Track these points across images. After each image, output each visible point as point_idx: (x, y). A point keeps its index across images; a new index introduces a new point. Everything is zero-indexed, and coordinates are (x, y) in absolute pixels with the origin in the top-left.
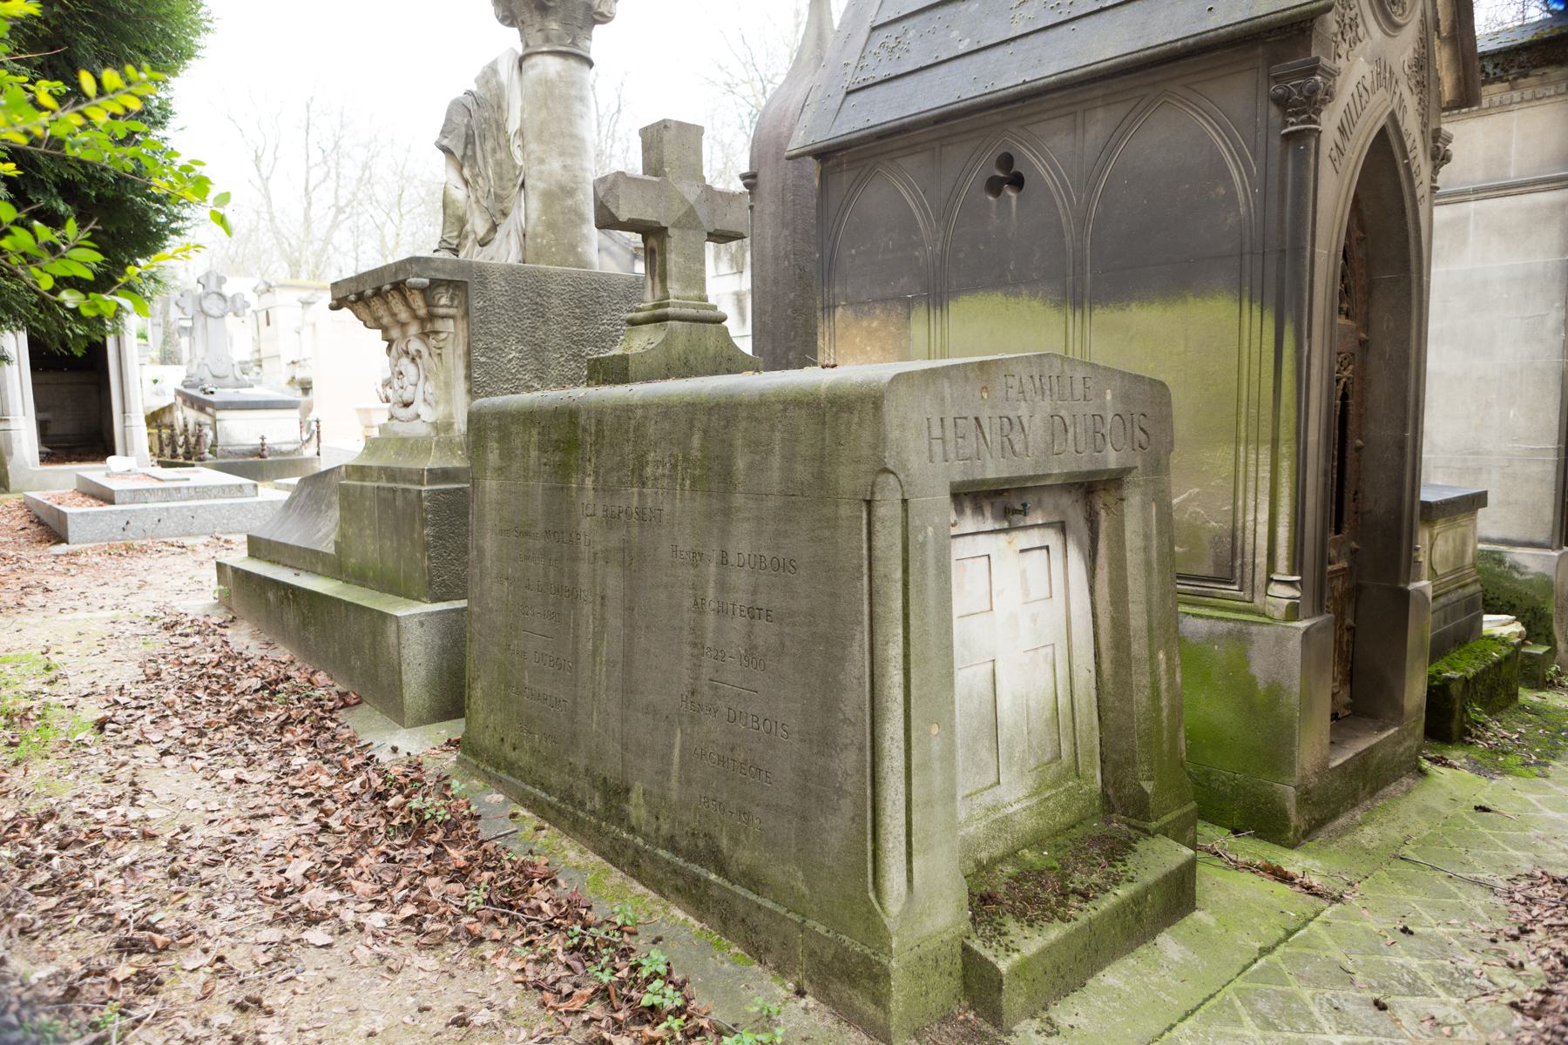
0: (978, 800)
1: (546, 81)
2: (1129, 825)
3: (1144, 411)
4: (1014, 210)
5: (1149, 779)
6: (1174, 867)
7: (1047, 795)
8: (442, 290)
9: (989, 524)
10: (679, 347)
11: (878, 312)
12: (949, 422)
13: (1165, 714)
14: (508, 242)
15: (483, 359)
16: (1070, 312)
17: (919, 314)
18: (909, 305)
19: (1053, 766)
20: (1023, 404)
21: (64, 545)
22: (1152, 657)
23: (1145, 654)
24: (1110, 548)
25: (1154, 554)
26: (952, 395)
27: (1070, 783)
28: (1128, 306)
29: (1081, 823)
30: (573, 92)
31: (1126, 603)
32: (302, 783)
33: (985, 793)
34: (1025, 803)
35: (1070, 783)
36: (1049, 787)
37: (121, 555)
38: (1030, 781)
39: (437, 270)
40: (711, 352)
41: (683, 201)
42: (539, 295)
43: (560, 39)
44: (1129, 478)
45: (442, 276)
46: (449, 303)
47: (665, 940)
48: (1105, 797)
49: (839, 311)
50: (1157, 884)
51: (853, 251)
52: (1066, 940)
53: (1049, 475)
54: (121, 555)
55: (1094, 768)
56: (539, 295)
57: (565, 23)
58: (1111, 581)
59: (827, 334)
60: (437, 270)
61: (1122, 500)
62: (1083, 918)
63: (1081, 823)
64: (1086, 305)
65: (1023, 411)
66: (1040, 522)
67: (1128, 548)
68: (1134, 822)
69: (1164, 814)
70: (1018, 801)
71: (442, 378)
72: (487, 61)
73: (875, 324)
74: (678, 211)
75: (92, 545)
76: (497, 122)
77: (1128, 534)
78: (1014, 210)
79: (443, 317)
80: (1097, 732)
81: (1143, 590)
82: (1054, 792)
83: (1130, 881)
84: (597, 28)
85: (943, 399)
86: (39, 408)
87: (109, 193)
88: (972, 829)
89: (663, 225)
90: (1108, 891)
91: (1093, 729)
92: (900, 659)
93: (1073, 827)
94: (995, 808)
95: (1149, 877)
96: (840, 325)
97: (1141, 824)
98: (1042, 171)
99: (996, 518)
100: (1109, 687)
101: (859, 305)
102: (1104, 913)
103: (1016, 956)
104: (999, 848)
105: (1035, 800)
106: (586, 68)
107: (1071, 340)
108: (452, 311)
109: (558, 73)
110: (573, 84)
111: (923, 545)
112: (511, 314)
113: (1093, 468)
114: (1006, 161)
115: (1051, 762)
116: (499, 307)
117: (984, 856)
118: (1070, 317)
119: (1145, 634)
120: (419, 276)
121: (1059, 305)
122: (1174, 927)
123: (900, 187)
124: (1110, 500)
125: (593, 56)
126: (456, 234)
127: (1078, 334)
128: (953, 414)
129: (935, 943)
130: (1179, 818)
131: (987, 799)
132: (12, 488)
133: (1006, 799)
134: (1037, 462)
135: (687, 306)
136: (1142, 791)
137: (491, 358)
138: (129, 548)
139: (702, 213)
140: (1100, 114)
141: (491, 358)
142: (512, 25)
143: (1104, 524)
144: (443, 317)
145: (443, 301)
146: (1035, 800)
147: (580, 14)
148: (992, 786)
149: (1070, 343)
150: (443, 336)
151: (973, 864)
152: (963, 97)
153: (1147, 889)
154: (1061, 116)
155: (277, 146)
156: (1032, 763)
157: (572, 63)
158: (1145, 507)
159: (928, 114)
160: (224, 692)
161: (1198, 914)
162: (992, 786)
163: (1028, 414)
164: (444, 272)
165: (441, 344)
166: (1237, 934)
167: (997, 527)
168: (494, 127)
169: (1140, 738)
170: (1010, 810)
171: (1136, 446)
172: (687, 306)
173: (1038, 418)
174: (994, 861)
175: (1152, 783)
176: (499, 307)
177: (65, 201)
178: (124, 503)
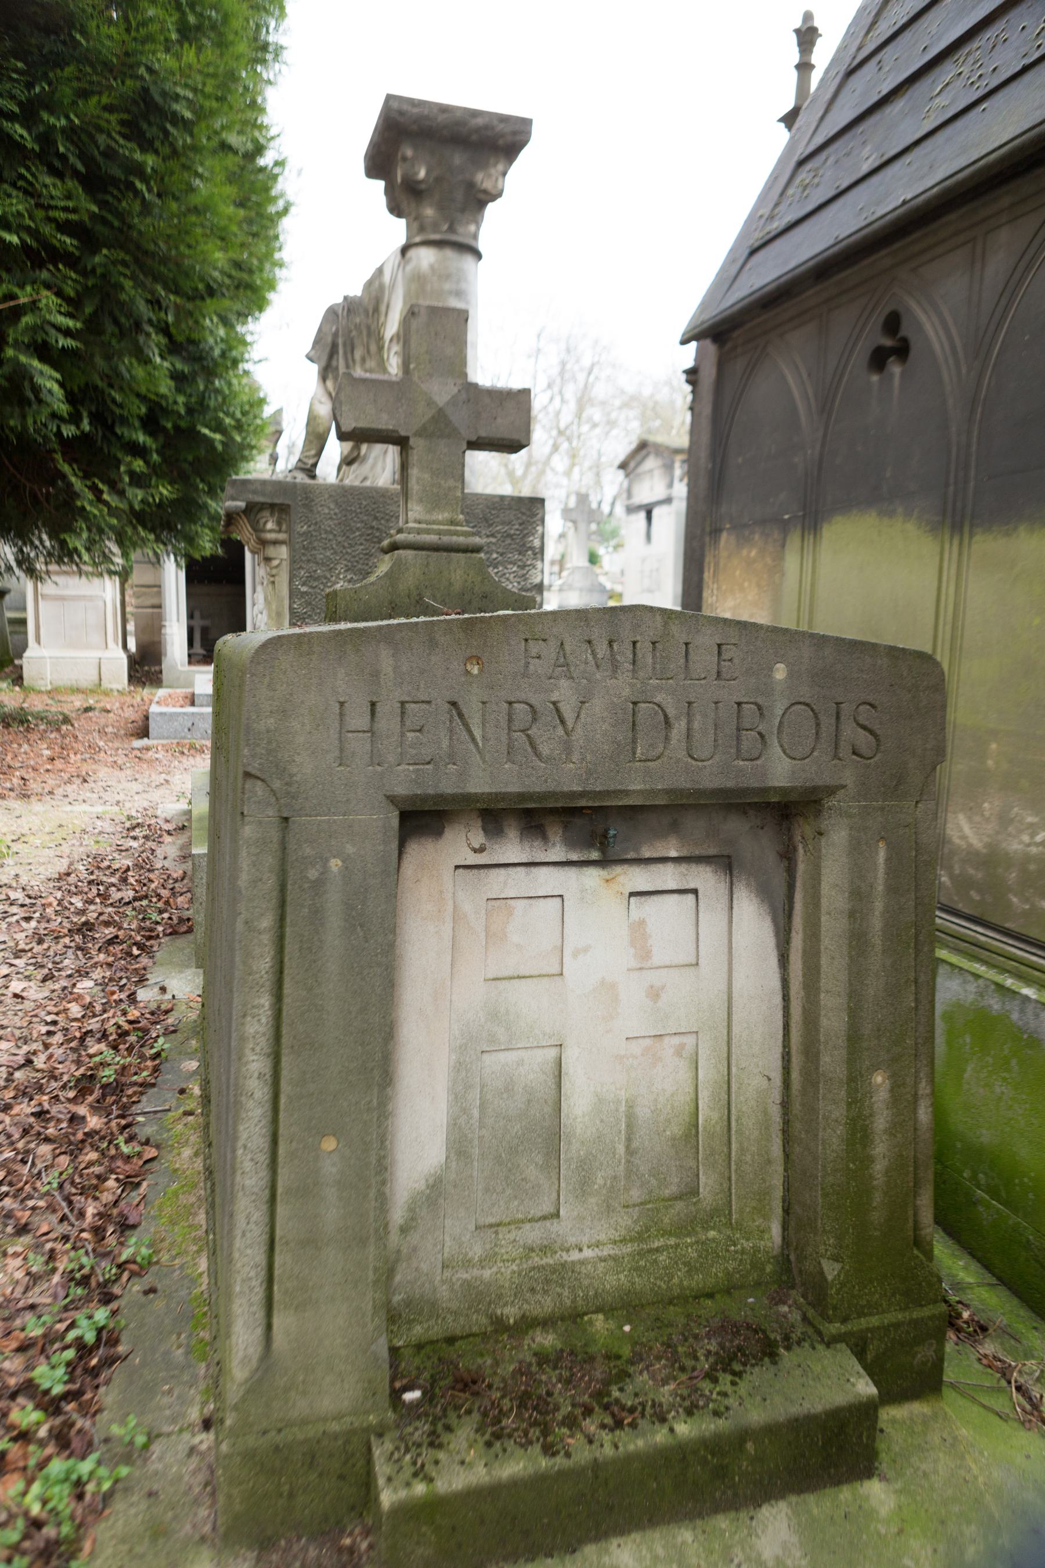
0: (507, 1236)
1: (419, 277)
2: (805, 1318)
3: (870, 698)
4: (896, 392)
5: (836, 1259)
6: (819, 1408)
7: (656, 1244)
8: (266, 513)
9: (557, 852)
10: (409, 580)
11: (757, 537)
12: (388, 708)
13: (879, 1167)
14: (384, 460)
15: (304, 589)
16: (947, 537)
17: (794, 540)
18: (785, 528)
19: (680, 1205)
20: (564, 683)
21: (146, 739)
22: (855, 1079)
23: (840, 1072)
24: (806, 905)
25: (876, 923)
26: (396, 668)
27: (712, 1234)
28: (1015, 529)
29: (728, 1291)
30: (447, 286)
31: (818, 990)
32: (55, 1010)
33: (527, 1226)
34: (607, 1251)
35: (712, 1234)
36: (666, 1233)
37: (183, 753)
38: (625, 1221)
39: (255, 492)
40: (457, 587)
41: (430, 403)
42: (376, 518)
43: (435, 227)
44: (832, 802)
45: (260, 499)
46: (275, 527)
47: (159, 1294)
48: (784, 1262)
49: (724, 535)
50: (771, 1430)
51: (740, 460)
52: (537, 1483)
53: (626, 793)
54: (183, 753)
55: (766, 1217)
56: (376, 518)
57: (441, 207)
58: (804, 951)
59: (712, 565)
60: (255, 492)
61: (821, 834)
62: (581, 1453)
63: (728, 1291)
64: (966, 529)
65: (565, 693)
66: (673, 854)
67: (823, 911)
68: (811, 1313)
69: (861, 1314)
70: (598, 1244)
71: (274, 607)
72: (378, 266)
73: (753, 553)
74: (423, 415)
75: (164, 742)
76: (368, 328)
77: (825, 888)
78: (896, 392)
79: (275, 543)
80: (778, 1168)
81: (843, 976)
82: (672, 1241)
83: (717, 1414)
84: (490, 206)
85: (376, 674)
86: (190, 616)
87: (183, 424)
88: (487, 1274)
89: (403, 433)
90: (663, 1420)
91: (769, 1162)
92: (264, 1043)
93: (710, 1296)
94: (545, 1249)
95: (756, 1416)
96: (724, 554)
97: (817, 1321)
98: (931, 334)
99: (571, 843)
100: (796, 1108)
101: (740, 528)
102: (629, 1459)
103: (420, 1488)
104: (545, 1305)
105: (628, 1249)
106: (469, 260)
107: (945, 578)
108: (282, 536)
109: (432, 267)
110: (448, 277)
111: (318, 885)
112: (340, 539)
113: (730, 784)
114: (893, 323)
115: (679, 1197)
116: (326, 532)
117: (511, 1313)
118: (947, 546)
119: (842, 1042)
120: (233, 499)
121: (935, 529)
122: (811, 1498)
123: (786, 372)
124: (808, 830)
125: (482, 246)
126: (313, 452)
127: (953, 572)
128: (399, 695)
129: (312, 1431)
130: (897, 1325)
131: (532, 1234)
132: (165, 683)
133: (572, 1240)
134: (589, 773)
135: (428, 532)
136: (822, 1273)
137: (314, 588)
138: (192, 747)
139: (459, 418)
140: (1004, 235)
141: (314, 588)
142: (399, 215)
143: (801, 867)
144: (275, 543)
145: (270, 525)
146: (628, 1249)
147: (459, 195)
148: (544, 1218)
149: (944, 584)
150: (275, 563)
151: (484, 1321)
152: (841, 237)
153: (743, 1435)
154: (958, 247)
155: (510, 374)
156: (636, 1194)
157: (449, 253)
158: (857, 848)
159: (803, 268)
160: (98, 900)
161: (874, 1490)
162: (544, 1218)
163: (574, 701)
164: (264, 495)
165: (274, 572)
166: (914, 1544)
167: (574, 857)
168: (365, 333)
169: (826, 1195)
170: (575, 1256)
171: (845, 751)
172: (428, 532)
173: (598, 705)
174: (528, 1324)
175: (837, 1266)
176: (326, 532)
177: (144, 434)
178: (202, 706)
